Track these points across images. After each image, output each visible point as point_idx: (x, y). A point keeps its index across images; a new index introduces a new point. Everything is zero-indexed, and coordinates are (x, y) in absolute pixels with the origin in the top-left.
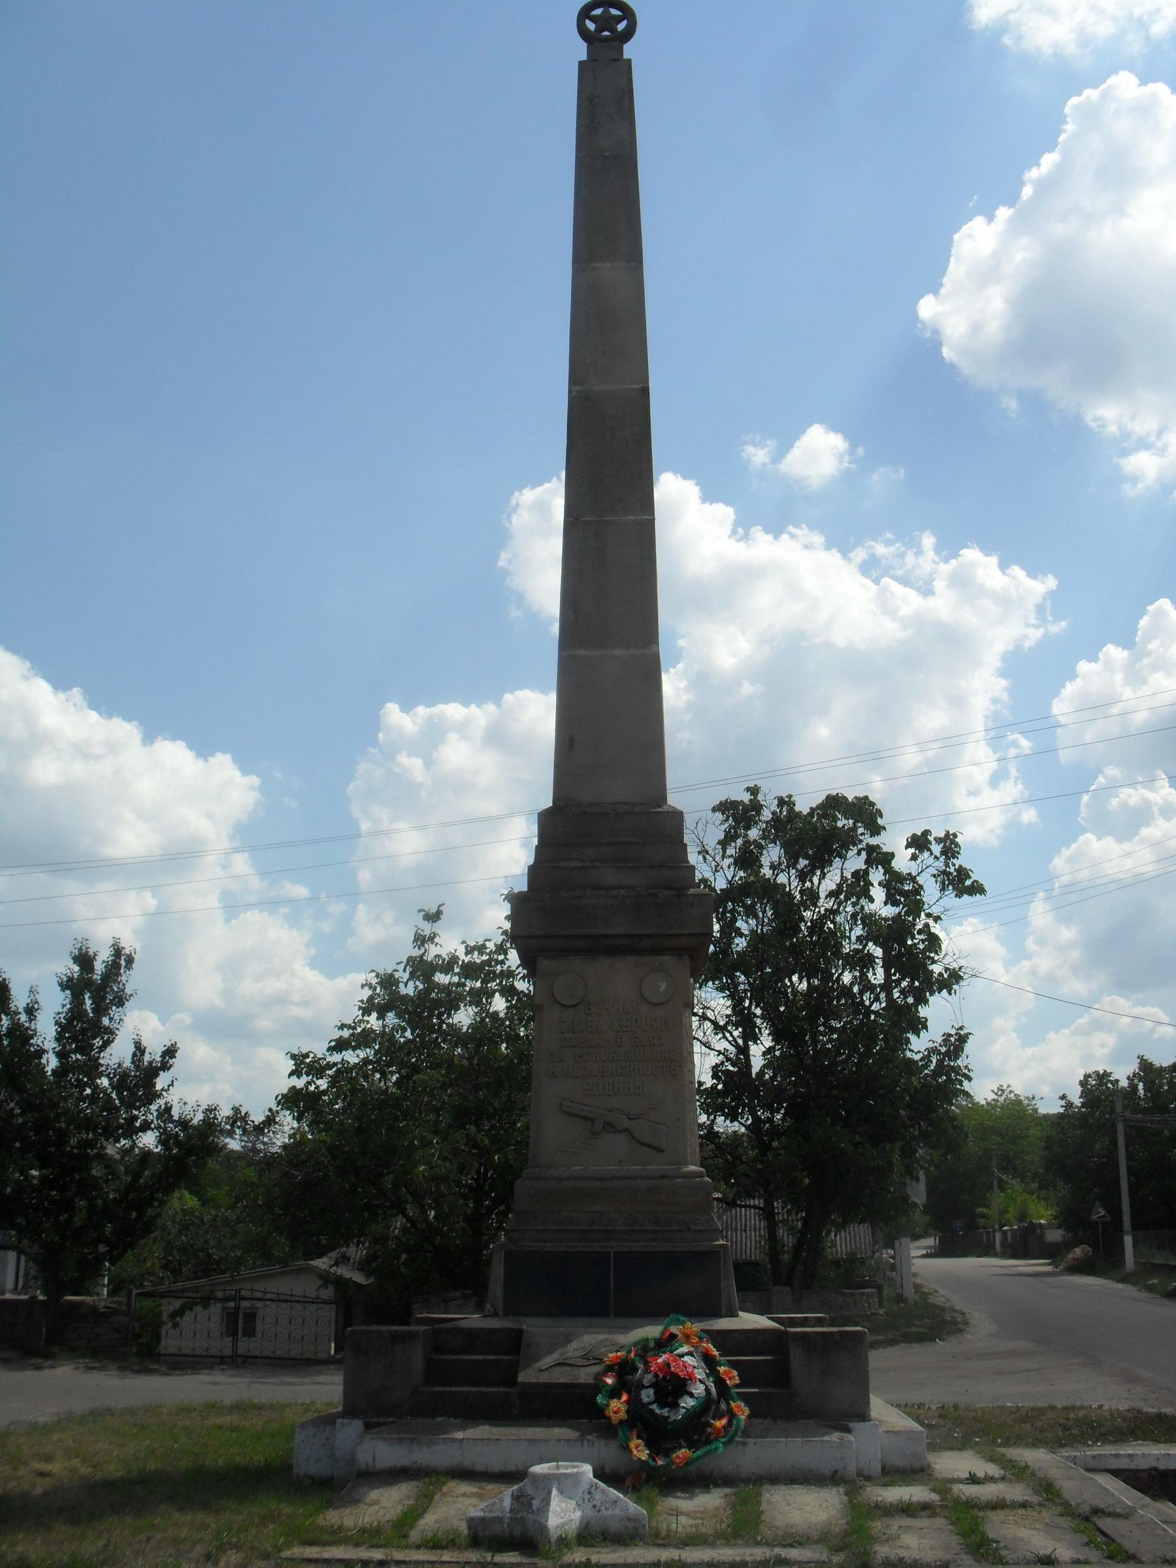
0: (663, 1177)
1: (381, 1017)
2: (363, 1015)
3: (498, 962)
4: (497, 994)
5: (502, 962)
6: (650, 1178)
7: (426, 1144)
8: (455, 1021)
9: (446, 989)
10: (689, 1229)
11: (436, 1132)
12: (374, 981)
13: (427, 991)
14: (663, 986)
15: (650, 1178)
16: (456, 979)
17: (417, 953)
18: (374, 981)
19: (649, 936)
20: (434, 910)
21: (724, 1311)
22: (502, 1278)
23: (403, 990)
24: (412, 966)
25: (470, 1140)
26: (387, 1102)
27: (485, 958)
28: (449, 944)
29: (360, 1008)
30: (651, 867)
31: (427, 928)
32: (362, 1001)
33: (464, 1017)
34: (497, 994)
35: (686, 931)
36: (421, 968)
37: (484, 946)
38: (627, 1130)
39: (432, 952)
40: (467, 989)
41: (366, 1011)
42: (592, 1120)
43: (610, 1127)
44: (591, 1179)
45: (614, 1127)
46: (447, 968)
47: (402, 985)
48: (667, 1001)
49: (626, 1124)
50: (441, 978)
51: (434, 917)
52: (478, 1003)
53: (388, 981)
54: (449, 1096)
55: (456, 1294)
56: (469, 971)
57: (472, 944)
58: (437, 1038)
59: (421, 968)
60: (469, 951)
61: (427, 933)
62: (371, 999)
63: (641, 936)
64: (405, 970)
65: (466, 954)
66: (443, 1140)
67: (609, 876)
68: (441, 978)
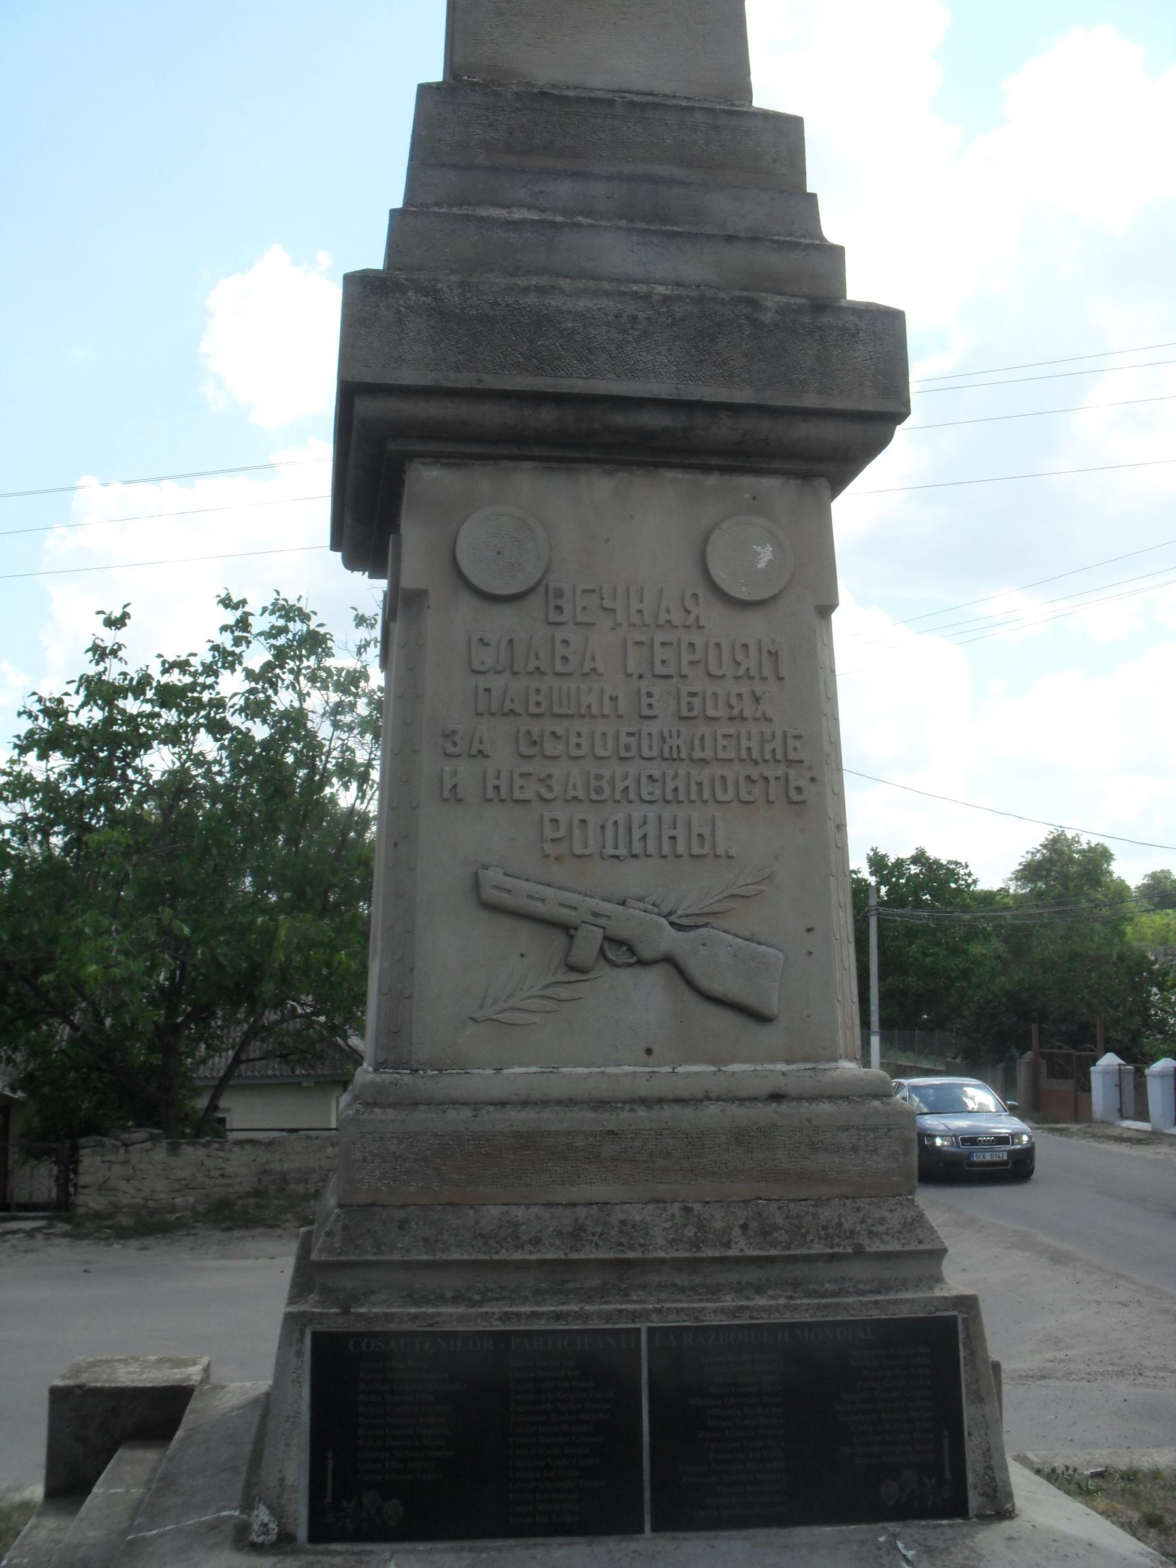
0: (776, 1097)
1: (43, 756)
2: (20, 755)
3: (205, 687)
4: (202, 730)
5: (211, 687)
6: (741, 1100)
7: (100, 932)
8: (146, 764)
9: (130, 720)
10: (859, 1252)
11: (115, 915)
12: (36, 708)
13: (109, 721)
14: (766, 555)
15: (741, 1100)
16: (147, 708)
17: (92, 670)
18: (36, 708)
19: (735, 409)
20: (117, 614)
21: (974, 1501)
22: (305, 1419)
23: (72, 720)
24: (87, 688)
25: (165, 931)
26: (51, 867)
27: (188, 679)
28: (141, 654)
29: (16, 746)
30: (730, 239)
31: (109, 637)
32: (18, 737)
33: (159, 761)
34: (202, 730)
35: (840, 404)
36: (98, 690)
37: (187, 663)
38: (669, 960)
39: (113, 671)
40: (162, 722)
41: (23, 750)
42: (567, 929)
43: (622, 951)
44: (570, 1103)
45: (632, 951)
46: (139, 688)
47: (71, 716)
48: (774, 598)
49: (669, 940)
50: (131, 705)
51: (116, 623)
52: (194, 677)
53: (55, 711)
54: (134, 866)
55: (141, 1134)
56: (168, 696)
57: (171, 658)
58: (119, 788)
59: (98, 690)
60: (167, 668)
61: (109, 644)
62: (31, 733)
63: (713, 408)
64: (77, 692)
65: (164, 672)
66: (126, 926)
67: (618, 254)
68: (131, 705)
